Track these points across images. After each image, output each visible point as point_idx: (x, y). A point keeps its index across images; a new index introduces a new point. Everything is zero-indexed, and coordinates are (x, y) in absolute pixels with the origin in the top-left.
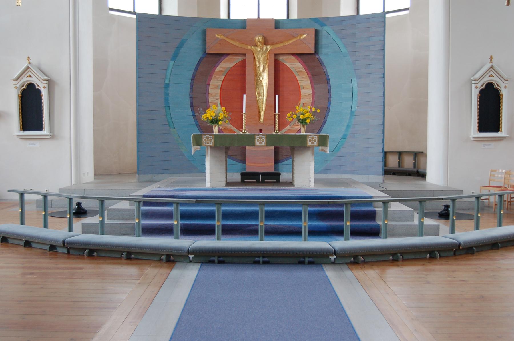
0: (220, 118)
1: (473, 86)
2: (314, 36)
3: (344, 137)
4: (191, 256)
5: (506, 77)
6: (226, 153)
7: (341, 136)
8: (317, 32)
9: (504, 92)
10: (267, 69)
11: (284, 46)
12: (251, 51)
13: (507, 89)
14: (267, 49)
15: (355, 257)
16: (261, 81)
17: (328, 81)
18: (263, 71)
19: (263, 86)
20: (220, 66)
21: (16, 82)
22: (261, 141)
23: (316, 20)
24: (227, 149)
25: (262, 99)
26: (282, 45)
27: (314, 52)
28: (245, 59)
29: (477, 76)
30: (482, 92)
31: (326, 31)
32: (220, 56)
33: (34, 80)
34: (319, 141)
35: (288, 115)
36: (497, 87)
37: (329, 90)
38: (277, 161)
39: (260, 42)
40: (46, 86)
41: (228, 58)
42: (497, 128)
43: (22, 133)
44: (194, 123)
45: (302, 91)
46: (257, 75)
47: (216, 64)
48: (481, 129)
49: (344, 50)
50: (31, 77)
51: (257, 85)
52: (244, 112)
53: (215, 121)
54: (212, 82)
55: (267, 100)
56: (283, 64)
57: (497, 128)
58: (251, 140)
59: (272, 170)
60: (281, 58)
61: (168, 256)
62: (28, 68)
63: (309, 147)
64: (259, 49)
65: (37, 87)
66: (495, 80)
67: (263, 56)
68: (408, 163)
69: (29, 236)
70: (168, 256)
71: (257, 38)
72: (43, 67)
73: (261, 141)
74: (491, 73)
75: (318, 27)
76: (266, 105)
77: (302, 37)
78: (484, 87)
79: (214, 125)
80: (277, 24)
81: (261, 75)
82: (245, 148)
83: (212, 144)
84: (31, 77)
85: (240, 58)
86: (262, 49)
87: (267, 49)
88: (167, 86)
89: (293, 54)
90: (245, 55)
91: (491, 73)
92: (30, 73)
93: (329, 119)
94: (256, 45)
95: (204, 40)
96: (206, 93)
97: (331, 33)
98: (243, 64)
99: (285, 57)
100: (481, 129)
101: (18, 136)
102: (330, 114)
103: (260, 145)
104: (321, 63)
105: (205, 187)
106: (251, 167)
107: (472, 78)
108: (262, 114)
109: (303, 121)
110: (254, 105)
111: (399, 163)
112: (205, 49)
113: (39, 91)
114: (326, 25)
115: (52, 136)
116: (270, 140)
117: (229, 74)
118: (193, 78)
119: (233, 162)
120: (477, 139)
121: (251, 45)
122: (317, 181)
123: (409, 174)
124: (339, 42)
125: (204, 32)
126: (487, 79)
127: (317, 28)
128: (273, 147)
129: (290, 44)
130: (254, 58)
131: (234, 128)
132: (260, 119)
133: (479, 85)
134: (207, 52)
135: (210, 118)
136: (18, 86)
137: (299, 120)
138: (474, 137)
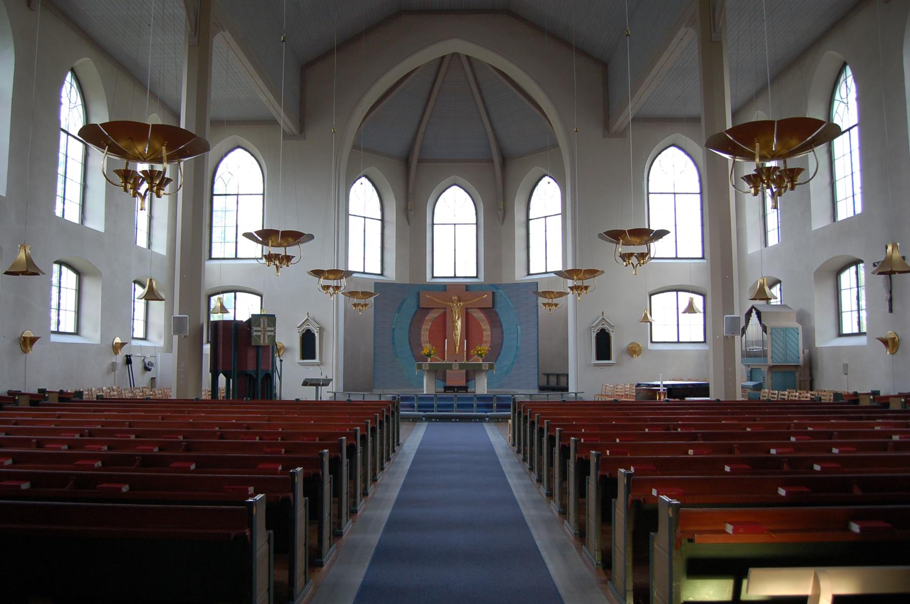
0: (432, 353)
1: (592, 331)
2: (491, 296)
3: (513, 363)
4: (424, 419)
5: (612, 324)
6: (436, 374)
8: (494, 294)
9: (612, 335)
12: (450, 306)
14: (460, 305)
15: (498, 419)
17: (501, 326)
18: (458, 319)
19: (457, 329)
20: (429, 316)
22: (456, 367)
23: (493, 285)
24: (436, 371)
25: (457, 338)
27: (491, 306)
28: (446, 312)
29: (594, 325)
30: (597, 334)
31: (500, 292)
32: (428, 310)
33: (311, 327)
34: (489, 367)
35: (472, 351)
37: (502, 332)
38: (467, 381)
39: (456, 300)
40: (318, 331)
41: (435, 310)
42: (609, 358)
43: (301, 361)
44: (411, 354)
45: (484, 332)
46: (454, 322)
47: (425, 315)
48: (598, 358)
50: (309, 325)
51: (454, 328)
52: (446, 349)
53: (429, 355)
55: (460, 339)
56: (472, 315)
57: (609, 358)
58: (450, 366)
59: (464, 385)
61: (413, 419)
62: (307, 319)
63: (484, 371)
65: (312, 332)
66: (606, 326)
67: (458, 309)
68: (553, 382)
70: (413, 419)
71: (453, 298)
72: (316, 319)
73: (456, 367)
75: (495, 291)
77: (484, 297)
79: (428, 358)
80: (467, 287)
81: (456, 322)
82: (446, 371)
83: (427, 368)
84: (309, 325)
85: (442, 311)
86: (457, 305)
87: (460, 305)
88: (394, 330)
89: (478, 308)
90: (445, 308)
92: (308, 323)
94: (453, 302)
95: (418, 299)
96: (419, 334)
97: (503, 294)
98: (445, 314)
100: (598, 358)
101: (299, 363)
103: (338, 531)
104: (497, 314)
106: (449, 383)
108: (457, 348)
109: (481, 355)
110: (452, 344)
111: (557, 382)
112: (419, 304)
113: (314, 335)
116: (462, 366)
119: (439, 381)
120: (595, 365)
121: (449, 302)
122: (487, 392)
123: (554, 389)
125: (418, 294)
126: (600, 327)
127: (493, 291)
128: (465, 371)
130: (452, 311)
131: (438, 358)
133: (596, 330)
135: (426, 353)
136: (300, 331)
137: (478, 355)
138: (594, 364)
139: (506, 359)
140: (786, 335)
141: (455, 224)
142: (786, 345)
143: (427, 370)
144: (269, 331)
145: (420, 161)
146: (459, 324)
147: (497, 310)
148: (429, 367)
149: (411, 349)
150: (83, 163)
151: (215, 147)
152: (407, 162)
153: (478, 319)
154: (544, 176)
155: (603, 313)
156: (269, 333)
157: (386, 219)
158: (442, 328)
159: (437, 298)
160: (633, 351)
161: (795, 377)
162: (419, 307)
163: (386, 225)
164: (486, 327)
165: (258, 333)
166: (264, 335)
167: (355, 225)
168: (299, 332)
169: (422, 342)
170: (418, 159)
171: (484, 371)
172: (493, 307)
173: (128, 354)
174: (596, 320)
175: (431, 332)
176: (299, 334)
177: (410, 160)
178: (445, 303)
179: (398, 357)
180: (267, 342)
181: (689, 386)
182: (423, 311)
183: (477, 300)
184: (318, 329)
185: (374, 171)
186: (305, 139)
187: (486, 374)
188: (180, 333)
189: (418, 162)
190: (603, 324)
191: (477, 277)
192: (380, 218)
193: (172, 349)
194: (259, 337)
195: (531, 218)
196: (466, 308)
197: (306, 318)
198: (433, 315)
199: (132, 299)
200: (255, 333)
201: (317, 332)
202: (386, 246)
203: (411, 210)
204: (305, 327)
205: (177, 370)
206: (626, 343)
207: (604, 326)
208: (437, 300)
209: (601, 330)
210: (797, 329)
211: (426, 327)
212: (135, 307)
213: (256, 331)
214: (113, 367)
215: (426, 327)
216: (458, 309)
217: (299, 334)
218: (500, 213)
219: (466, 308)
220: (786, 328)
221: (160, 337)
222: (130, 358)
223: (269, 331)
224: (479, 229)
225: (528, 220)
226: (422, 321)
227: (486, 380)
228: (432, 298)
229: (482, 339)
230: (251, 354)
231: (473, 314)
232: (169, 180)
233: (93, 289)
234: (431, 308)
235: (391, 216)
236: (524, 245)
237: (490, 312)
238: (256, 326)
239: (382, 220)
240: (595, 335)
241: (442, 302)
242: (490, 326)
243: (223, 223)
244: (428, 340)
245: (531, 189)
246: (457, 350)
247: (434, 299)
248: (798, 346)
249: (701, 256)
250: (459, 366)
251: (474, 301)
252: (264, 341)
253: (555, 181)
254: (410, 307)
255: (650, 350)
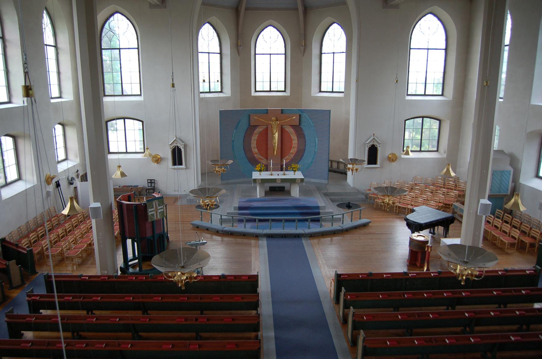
2: (299, 118)
3: (312, 162)
7: (310, 162)
8: (300, 115)
9: (379, 149)
10: (277, 132)
11: (285, 122)
13: (380, 147)
16: (275, 137)
17: (305, 138)
18: (276, 132)
19: (275, 139)
21: (170, 146)
26: (284, 121)
27: (298, 125)
28: (268, 127)
29: (368, 142)
30: (369, 148)
31: (305, 115)
32: (256, 127)
33: (179, 145)
36: (376, 146)
37: (305, 141)
39: (274, 120)
40: (183, 147)
41: (260, 127)
42: (375, 163)
43: (173, 167)
46: (273, 134)
47: (254, 129)
49: (312, 124)
50: (177, 143)
54: (253, 138)
55: (277, 146)
56: (285, 129)
57: (375, 163)
60: (284, 126)
63: (297, 183)
64: (274, 123)
65: (179, 147)
66: (375, 143)
67: (276, 126)
69: (198, 225)
74: (374, 141)
75: (301, 114)
76: (277, 147)
78: (370, 146)
81: (275, 134)
84: (177, 143)
85: (265, 127)
88: (233, 141)
89: (289, 125)
91: (374, 141)
93: (305, 154)
94: (273, 121)
95: (249, 121)
98: (267, 129)
99: (286, 126)
102: (305, 152)
104: (302, 130)
105: (255, 198)
107: (366, 143)
111: (338, 166)
112: (250, 124)
113: (181, 149)
114: (304, 113)
115: (187, 168)
117: (260, 134)
118: (245, 137)
124: (310, 121)
125: (249, 116)
126: (372, 143)
127: (300, 114)
129: (288, 121)
132: (274, 154)
133: (368, 146)
134: (251, 125)
136: (171, 147)
139: (307, 158)
140: (502, 175)
141: (270, 54)
142: (501, 182)
143: (259, 183)
144: (160, 209)
145: (247, 9)
146: (276, 135)
147: (302, 127)
148: (261, 182)
149: (245, 153)
150: (3, 53)
151: (100, 14)
152: (237, 10)
153: (289, 132)
154: (334, 23)
155: (374, 135)
156: (160, 211)
157: (223, 52)
158: (265, 136)
159: (262, 119)
160: (393, 159)
161: (503, 201)
162: (249, 125)
163: (224, 57)
164: (294, 137)
165: (152, 213)
166: (157, 213)
167: (202, 59)
168: (170, 148)
169: (252, 148)
170: (245, 8)
171: (297, 183)
172: (300, 124)
173: (57, 181)
174: (369, 139)
175: (258, 141)
176: (170, 149)
177: (239, 9)
178: (267, 122)
179: (236, 159)
180: (159, 217)
181: (440, 221)
182: (252, 128)
183: (288, 120)
184: (183, 146)
185: (214, 19)
186: (166, 8)
187: (298, 185)
188: (96, 218)
189: (245, 10)
190: (373, 142)
191: (285, 91)
192: (219, 52)
193: (85, 161)
194: (153, 215)
195: (323, 52)
196: (281, 125)
197: (174, 139)
198: (259, 130)
199: (55, 148)
200: (150, 213)
201: (183, 148)
202: (224, 71)
203: (240, 46)
204: (175, 144)
205: (97, 238)
206: (388, 153)
207: (374, 143)
208: (262, 120)
209: (372, 145)
210: (510, 171)
211: (255, 138)
212: (57, 141)
213: (151, 212)
214: (48, 194)
215: (255, 138)
216: (276, 126)
217: (170, 149)
218: (302, 48)
219: (281, 125)
220: (503, 171)
221: (77, 157)
222: (59, 183)
223: (160, 209)
224: (287, 58)
225: (321, 53)
226: (251, 134)
227: (298, 188)
228: (258, 118)
229: (292, 145)
230: (148, 226)
231: (286, 129)
232: (86, 224)
233: (26, 147)
234: (257, 126)
235: (227, 51)
236: (318, 71)
237: (298, 128)
238: (151, 208)
239: (221, 53)
240: (368, 149)
241: (266, 121)
242: (297, 137)
243: (113, 62)
244: (256, 146)
245: (324, 31)
246: (275, 153)
247: (260, 119)
248: (509, 182)
249: (440, 93)
250: (281, 180)
251: (286, 120)
252: (157, 217)
253: (342, 28)
254: (244, 125)
255: (402, 158)
